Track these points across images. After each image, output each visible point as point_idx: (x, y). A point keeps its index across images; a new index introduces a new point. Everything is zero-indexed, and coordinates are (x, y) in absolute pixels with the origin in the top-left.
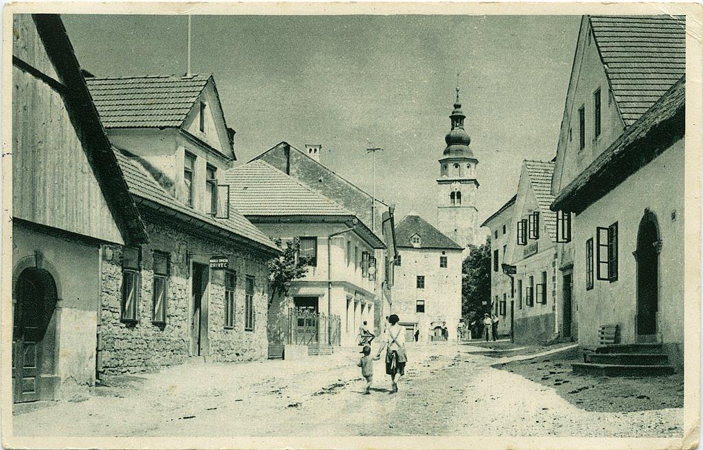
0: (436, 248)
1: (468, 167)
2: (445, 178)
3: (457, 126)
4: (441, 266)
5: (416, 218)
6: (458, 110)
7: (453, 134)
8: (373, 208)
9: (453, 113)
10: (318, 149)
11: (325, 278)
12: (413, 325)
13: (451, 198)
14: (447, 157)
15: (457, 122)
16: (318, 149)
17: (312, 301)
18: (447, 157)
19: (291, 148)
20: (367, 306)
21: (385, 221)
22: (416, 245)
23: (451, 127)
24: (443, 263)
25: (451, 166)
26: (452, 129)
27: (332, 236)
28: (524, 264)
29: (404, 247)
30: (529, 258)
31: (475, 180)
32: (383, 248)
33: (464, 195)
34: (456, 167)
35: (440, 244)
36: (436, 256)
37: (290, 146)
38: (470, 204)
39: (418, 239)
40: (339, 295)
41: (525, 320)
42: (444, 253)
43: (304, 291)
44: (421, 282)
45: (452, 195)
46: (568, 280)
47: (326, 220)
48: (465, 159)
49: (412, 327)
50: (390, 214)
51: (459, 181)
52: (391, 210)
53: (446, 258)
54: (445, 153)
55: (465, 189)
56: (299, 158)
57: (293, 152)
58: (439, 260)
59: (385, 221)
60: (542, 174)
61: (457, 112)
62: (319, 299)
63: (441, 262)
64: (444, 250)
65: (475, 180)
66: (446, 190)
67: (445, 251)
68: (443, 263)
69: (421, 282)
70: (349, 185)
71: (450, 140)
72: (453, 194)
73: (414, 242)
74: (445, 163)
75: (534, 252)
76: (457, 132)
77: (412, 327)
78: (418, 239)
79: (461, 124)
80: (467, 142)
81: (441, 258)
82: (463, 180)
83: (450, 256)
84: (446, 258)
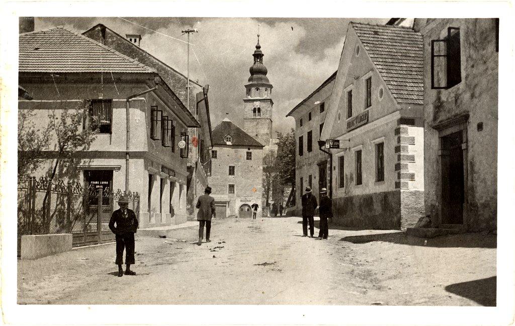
0: (243, 145)
1: (266, 90)
2: (249, 98)
3: (257, 62)
4: (247, 159)
5: (229, 124)
6: (258, 50)
7: (255, 67)
8: (187, 88)
9: (255, 52)
10: (138, 39)
11: (123, 149)
12: (226, 203)
13: (254, 112)
14: (251, 83)
15: (258, 59)
16: (138, 39)
17: (106, 175)
18: (251, 83)
19: (107, 29)
20: (177, 185)
21: (199, 102)
22: (229, 143)
23: (253, 63)
24: (249, 156)
25: (253, 89)
26: (255, 63)
27: (131, 97)
28: (348, 139)
29: (220, 144)
30: (352, 132)
31: (271, 100)
32: (197, 127)
33: (263, 110)
34: (257, 90)
35: (244, 141)
36: (243, 152)
37: (106, 27)
38: (268, 116)
39: (230, 138)
40: (137, 168)
41: (349, 200)
42: (249, 149)
43: (97, 163)
44: (232, 171)
45: (254, 110)
46: (380, 158)
47: (123, 78)
48: (263, 85)
49: (225, 205)
50: (204, 94)
51: (259, 100)
52: (205, 90)
53: (251, 153)
54: (249, 80)
55: (264, 106)
56: (115, 39)
57: (109, 34)
58: (246, 154)
59: (199, 102)
60: (372, 36)
61: (258, 51)
62: (114, 171)
63: (247, 156)
64: (249, 147)
65: (271, 100)
66: (250, 106)
67: (250, 148)
68: (249, 156)
69: (232, 171)
70: (164, 66)
71: (253, 71)
72: (255, 109)
73: (227, 141)
74: (249, 92)
75: (364, 122)
76: (258, 65)
77: (225, 205)
78: (230, 138)
79: (261, 60)
80: (265, 73)
81: (247, 153)
82: (262, 100)
83: (254, 152)
84: (251, 153)
